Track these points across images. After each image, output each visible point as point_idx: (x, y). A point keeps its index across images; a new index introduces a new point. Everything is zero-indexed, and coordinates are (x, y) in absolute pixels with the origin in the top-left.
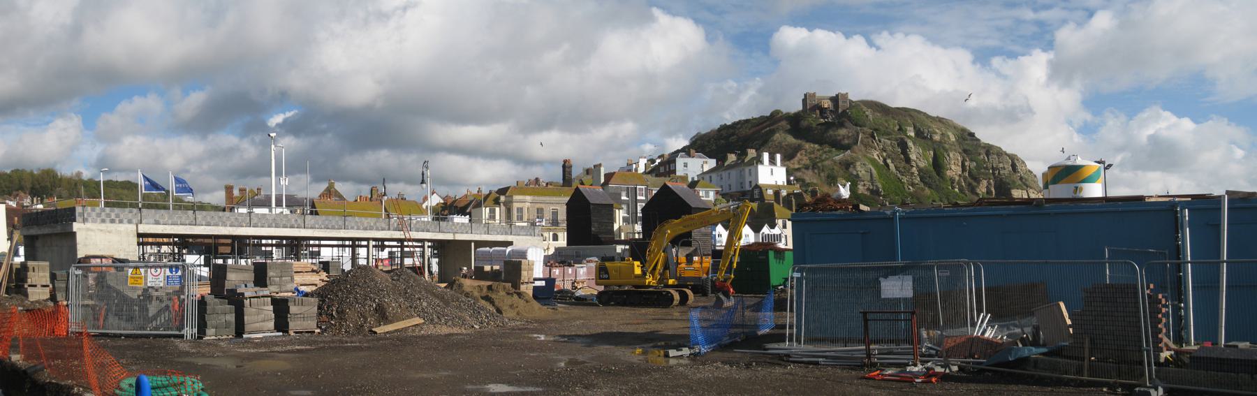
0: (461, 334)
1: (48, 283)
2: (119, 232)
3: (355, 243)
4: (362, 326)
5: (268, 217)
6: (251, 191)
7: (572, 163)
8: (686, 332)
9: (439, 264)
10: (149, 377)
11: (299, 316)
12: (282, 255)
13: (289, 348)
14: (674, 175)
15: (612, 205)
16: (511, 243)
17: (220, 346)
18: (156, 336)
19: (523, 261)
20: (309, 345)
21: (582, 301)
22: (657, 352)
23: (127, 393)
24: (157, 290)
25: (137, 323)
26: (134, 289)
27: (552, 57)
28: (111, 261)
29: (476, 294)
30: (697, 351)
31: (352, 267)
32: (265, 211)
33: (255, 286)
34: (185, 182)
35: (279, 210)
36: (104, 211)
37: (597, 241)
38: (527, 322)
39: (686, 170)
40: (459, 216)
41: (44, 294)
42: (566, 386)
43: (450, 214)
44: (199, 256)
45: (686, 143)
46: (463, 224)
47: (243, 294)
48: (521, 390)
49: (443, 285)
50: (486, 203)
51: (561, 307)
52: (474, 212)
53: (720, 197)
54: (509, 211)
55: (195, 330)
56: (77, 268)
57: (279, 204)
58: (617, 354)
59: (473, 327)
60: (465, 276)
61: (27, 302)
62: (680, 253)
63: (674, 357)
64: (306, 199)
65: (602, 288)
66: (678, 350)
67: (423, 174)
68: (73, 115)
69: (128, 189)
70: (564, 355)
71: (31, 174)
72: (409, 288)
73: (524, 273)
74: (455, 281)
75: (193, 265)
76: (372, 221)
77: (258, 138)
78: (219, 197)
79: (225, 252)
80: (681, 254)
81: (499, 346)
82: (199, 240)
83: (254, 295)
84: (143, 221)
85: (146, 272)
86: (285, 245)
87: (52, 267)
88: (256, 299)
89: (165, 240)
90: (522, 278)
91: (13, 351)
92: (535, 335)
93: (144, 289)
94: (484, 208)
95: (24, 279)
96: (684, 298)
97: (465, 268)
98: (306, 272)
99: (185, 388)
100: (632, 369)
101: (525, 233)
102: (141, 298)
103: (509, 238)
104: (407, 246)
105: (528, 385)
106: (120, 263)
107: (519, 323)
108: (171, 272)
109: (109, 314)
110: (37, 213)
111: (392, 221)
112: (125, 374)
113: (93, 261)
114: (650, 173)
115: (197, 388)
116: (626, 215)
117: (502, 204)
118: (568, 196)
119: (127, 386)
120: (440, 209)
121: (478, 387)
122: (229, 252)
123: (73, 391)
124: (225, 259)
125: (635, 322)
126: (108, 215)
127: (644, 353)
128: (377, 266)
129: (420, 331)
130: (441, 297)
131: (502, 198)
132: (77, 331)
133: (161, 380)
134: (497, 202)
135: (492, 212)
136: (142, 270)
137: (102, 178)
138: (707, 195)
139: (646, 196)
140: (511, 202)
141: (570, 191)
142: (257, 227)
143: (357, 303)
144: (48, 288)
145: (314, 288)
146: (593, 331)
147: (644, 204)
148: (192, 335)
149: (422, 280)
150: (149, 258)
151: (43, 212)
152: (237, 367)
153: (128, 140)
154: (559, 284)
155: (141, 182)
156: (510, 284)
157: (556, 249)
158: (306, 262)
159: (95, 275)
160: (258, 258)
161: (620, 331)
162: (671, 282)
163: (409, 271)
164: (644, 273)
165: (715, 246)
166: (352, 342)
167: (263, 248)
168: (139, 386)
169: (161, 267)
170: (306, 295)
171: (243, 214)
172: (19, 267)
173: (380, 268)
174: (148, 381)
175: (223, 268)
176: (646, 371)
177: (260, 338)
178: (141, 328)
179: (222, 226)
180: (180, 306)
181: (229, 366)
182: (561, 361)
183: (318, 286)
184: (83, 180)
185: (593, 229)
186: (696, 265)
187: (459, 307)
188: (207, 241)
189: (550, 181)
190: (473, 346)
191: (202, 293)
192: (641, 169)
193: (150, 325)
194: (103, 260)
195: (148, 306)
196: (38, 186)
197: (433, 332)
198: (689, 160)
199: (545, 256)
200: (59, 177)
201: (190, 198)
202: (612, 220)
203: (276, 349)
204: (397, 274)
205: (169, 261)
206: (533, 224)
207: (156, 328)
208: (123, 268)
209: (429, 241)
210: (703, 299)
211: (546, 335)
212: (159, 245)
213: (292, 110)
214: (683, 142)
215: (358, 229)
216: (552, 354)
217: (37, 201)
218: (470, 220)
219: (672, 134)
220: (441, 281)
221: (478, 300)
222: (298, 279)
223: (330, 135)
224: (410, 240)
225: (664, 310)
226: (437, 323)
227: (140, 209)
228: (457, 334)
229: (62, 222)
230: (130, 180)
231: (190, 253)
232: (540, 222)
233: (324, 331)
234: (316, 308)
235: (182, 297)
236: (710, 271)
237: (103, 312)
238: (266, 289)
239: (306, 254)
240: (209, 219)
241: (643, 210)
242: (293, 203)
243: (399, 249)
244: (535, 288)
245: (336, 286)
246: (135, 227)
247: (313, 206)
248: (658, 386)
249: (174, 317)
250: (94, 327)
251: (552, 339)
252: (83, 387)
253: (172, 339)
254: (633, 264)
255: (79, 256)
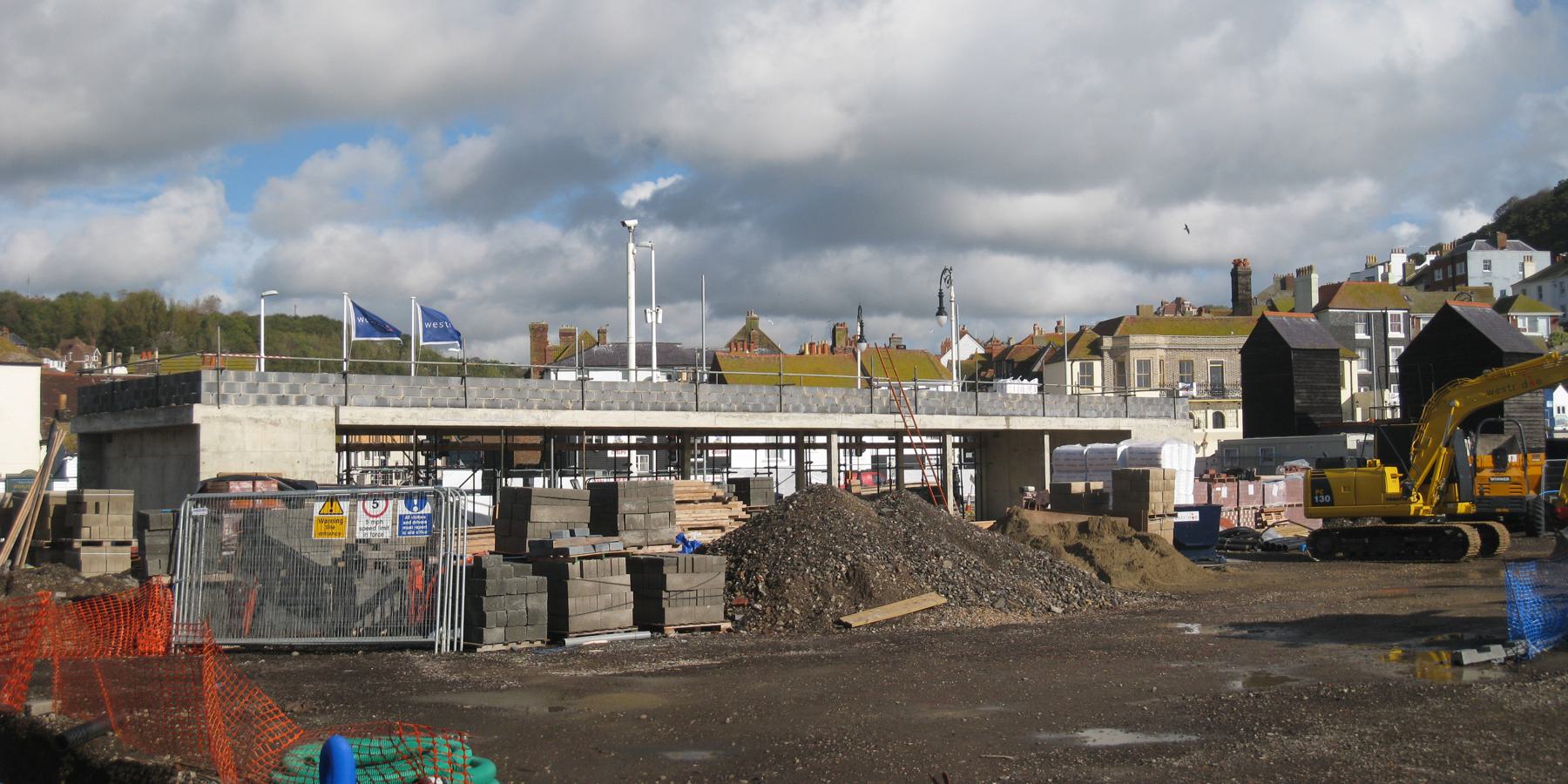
0: (1024, 626)
1: (130, 536)
2: (298, 424)
3: (802, 440)
4: (819, 613)
5: (619, 388)
6: (586, 335)
7: (1251, 265)
8: (1497, 612)
9: (977, 481)
10: (351, 741)
11: (686, 595)
12: (651, 467)
13: (665, 664)
14: (1463, 286)
15: (1338, 350)
16: (1125, 435)
17: (514, 665)
18: (370, 648)
19: (1152, 470)
20: (708, 657)
21: (1277, 552)
22: (1433, 655)
23: (300, 780)
24: (376, 547)
25: (329, 619)
26: (326, 545)
27: (1198, 50)
28: (275, 486)
29: (1055, 541)
30: (1521, 651)
31: (797, 488)
32: (614, 376)
33: (592, 532)
34: (444, 318)
35: (643, 375)
36: (264, 379)
37: (1306, 426)
38: (1163, 597)
39: (1489, 275)
40: (1018, 381)
41: (121, 561)
42: (1247, 730)
43: (999, 377)
44: (471, 472)
45: (1485, 219)
46: (1025, 397)
47: (565, 551)
48: (1152, 739)
49: (986, 524)
50: (1074, 352)
51: (1232, 565)
52: (1048, 371)
53: (1560, 330)
54: (1121, 368)
55: (460, 632)
56: (198, 502)
57: (643, 362)
58: (1351, 660)
59: (1049, 610)
60: (1031, 505)
61: (76, 579)
62: (1481, 449)
63: (1472, 665)
64: (701, 351)
65: (1318, 524)
66: (1480, 650)
67: (941, 295)
68: (205, 181)
69: (320, 333)
70: (1242, 664)
71: (106, 302)
72: (914, 532)
73: (1155, 497)
74: (1010, 515)
75: (458, 492)
76: (834, 395)
77: (600, 230)
78: (517, 349)
79: (530, 462)
80: (1483, 448)
81: (1104, 649)
82: (472, 439)
83: (591, 552)
84: (351, 400)
85: (353, 508)
86: (657, 447)
87: (139, 501)
88: (593, 561)
89: (398, 439)
90: (1152, 506)
91: (36, 692)
92: (1181, 625)
93: (347, 546)
94: (1068, 364)
95: (73, 530)
96: (1490, 540)
97: (1032, 488)
98: (701, 501)
99: (434, 761)
100: (1385, 692)
101: (1155, 414)
102: (342, 564)
103: (1122, 424)
104: (910, 445)
105: (1166, 730)
106: (295, 491)
107: (1145, 600)
108: (410, 507)
109: (267, 602)
110: (113, 384)
111: (878, 393)
112: (296, 737)
113: (236, 488)
114: (1413, 283)
115: (460, 760)
116: (1365, 371)
117: (1106, 354)
118: (1243, 334)
119: (302, 763)
120: (978, 367)
121: (1063, 735)
122: (538, 462)
123: (173, 779)
124: (527, 478)
125: (1390, 592)
126: (274, 389)
127: (1404, 658)
128: (848, 487)
129: (938, 621)
130: (982, 549)
131: (1107, 342)
132: (190, 641)
133: (380, 746)
134: (1096, 349)
135: (1087, 370)
136: (345, 505)
137: (263, 311)
138: (1534, 327)
139: (1407, 331)
140: (1126, 349)
141: (1249, 324)
142: (597, 408)
143: (808, 564)
144: (128, 548)
145: (718, 535)
146: (1303, 613)
147: (1402, 348)
148: (452, 643)
149: (941, 514)
150: (361, 478)
151: (126, 383)
152: (551, 709)
153: (323, 234)
154: (1228, 517)
155: (349, 317)
156: (1126, 520)
157: (1222, 445)
158: (702, 481)
159: (240, 516)
160: (599, 473)
161: (1358, 612)
162: (1462, 507)
163: (915, 496)
164: (1406, 492)
165: (1552, 431)
166: (798, 648)
167: (610, 454)
168: (327, 763)
169: (386, 497)
170: (702, 549)
171: (567, 382)
172: (64, 502)
173: (854, 490)
174: (349, 749)
175: (525, 496)
176: (1415, 695)
177: (601, 645)
178: (337, 633)
179: (522, 408)
180: (426, 581)
181: (533, 709)
182: (1234, 677)
183: (727, 531)
184: (221, 314)
185: (1297, 401)
186: (1515, 473)
187: (1018, 570)
188: (489, 440)
189: (1208, 303)
190: (1050, 651)
191: (477, 550)
192: (1396, 276)
193: (359, 624)
194: (259, 484)
195: (357, 582)
196: (118, 328)
197: (967, 623)
198: (1494, 255)
199: (1198, 460)
200: (168, 309)
201: (453, 351)
202: (1337, 382)
203: (638, 667)
204: (888, 502)
205: (406, 484)
206: (1172, 394)
207: (372, 631)
208: (303, 500)
209: (955, 432)
210: (1530, 541)
211: (1204, 624)
212: (385, 449)
213: (671, 175)
214: (1476, 219)
215: (809, 410)
216: (1217, 663)
217: (115, 359)
218: (1040, 389)
219: (1455, 200)
220: (980, 516)
221: (1059, 553)
222: (684, 516)
223: (748, 224)
224: (915, 432)
225: (1449, 568)
226: (974, 604)
227: (345, 375)
228: (1016, 626)
229: (168, 403)
230: (324, 314)
231: (451, 465)
232: (1187, 389)
233: (739, 625)
234: (722, 577)
235: (432, 560)
236: (1543, 483)
237: (252, 599)
238: (616, 539)
239: (701, 465)
240: (494, 394)
241: (1402, 360)
242: (672, 358)
243: (893, 451)
244: (1179, 527)
245: (764, 529)
246: (332, 413)
247: (715, 364)
248: (1440, 727)
249: (413, 605)
250: (229, 632)
251: (1215, 632)
252: (198, 770)
253: (408, 653)
254: (1384, 473)
255: (204, 477)
